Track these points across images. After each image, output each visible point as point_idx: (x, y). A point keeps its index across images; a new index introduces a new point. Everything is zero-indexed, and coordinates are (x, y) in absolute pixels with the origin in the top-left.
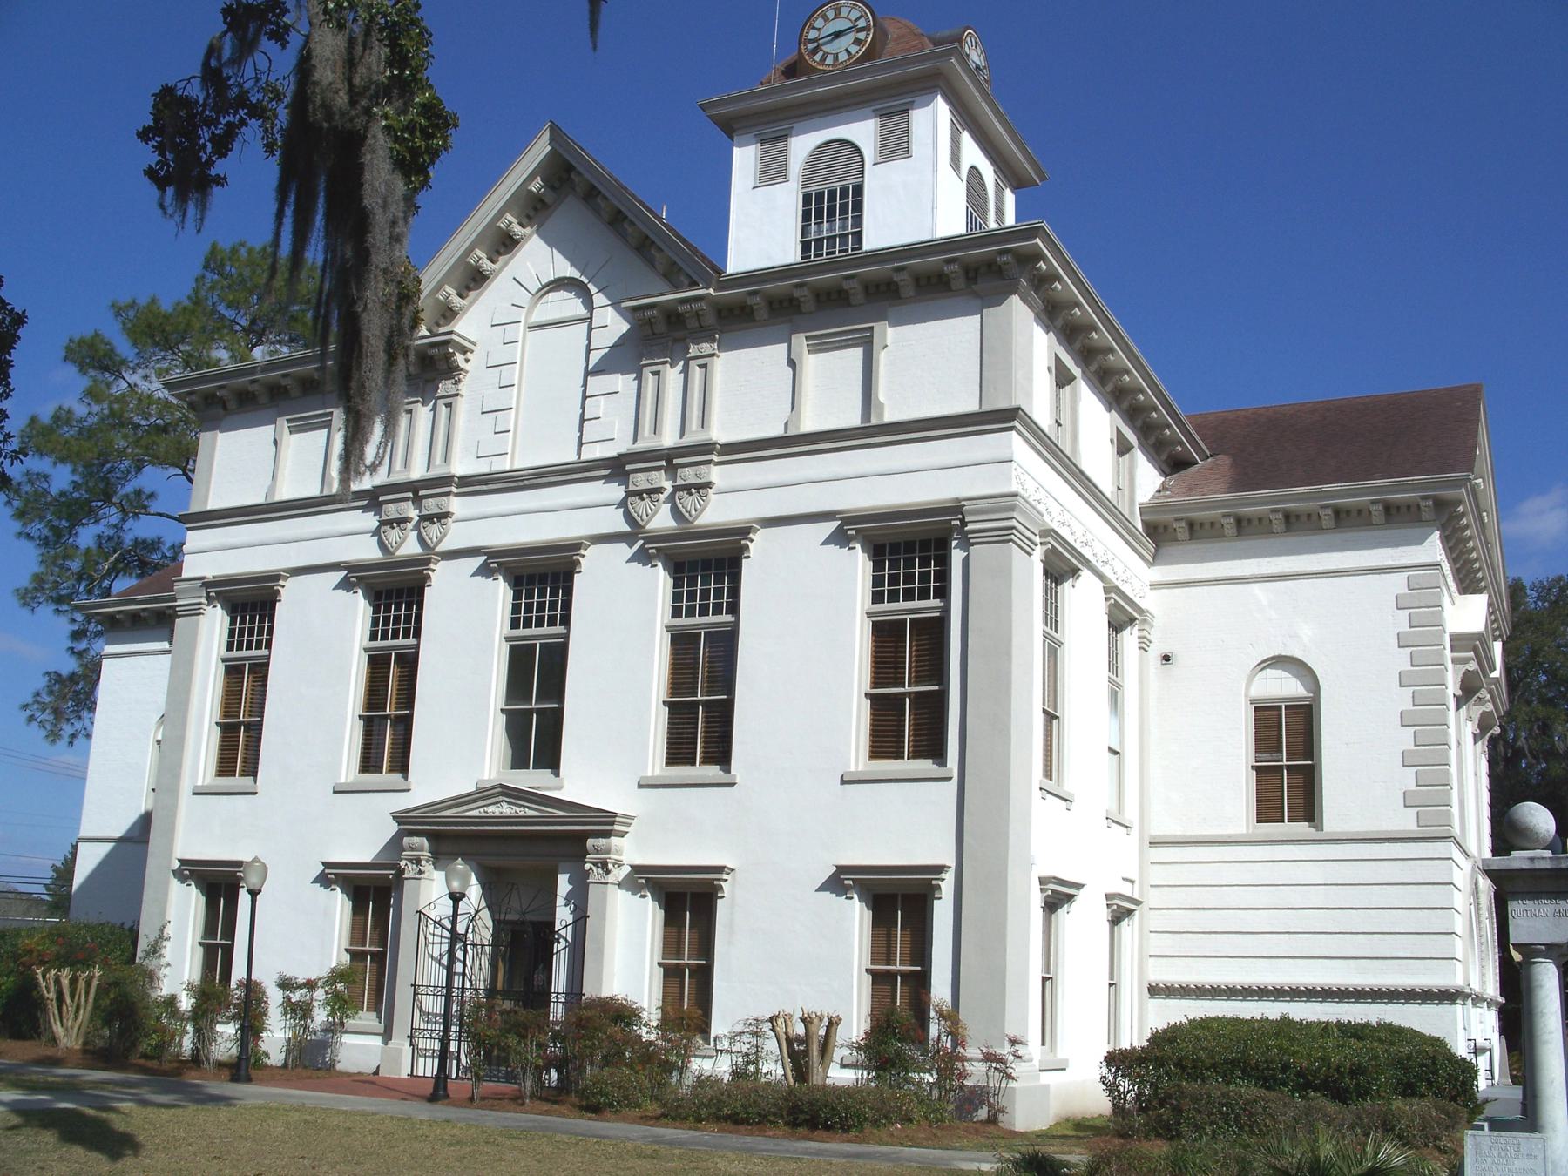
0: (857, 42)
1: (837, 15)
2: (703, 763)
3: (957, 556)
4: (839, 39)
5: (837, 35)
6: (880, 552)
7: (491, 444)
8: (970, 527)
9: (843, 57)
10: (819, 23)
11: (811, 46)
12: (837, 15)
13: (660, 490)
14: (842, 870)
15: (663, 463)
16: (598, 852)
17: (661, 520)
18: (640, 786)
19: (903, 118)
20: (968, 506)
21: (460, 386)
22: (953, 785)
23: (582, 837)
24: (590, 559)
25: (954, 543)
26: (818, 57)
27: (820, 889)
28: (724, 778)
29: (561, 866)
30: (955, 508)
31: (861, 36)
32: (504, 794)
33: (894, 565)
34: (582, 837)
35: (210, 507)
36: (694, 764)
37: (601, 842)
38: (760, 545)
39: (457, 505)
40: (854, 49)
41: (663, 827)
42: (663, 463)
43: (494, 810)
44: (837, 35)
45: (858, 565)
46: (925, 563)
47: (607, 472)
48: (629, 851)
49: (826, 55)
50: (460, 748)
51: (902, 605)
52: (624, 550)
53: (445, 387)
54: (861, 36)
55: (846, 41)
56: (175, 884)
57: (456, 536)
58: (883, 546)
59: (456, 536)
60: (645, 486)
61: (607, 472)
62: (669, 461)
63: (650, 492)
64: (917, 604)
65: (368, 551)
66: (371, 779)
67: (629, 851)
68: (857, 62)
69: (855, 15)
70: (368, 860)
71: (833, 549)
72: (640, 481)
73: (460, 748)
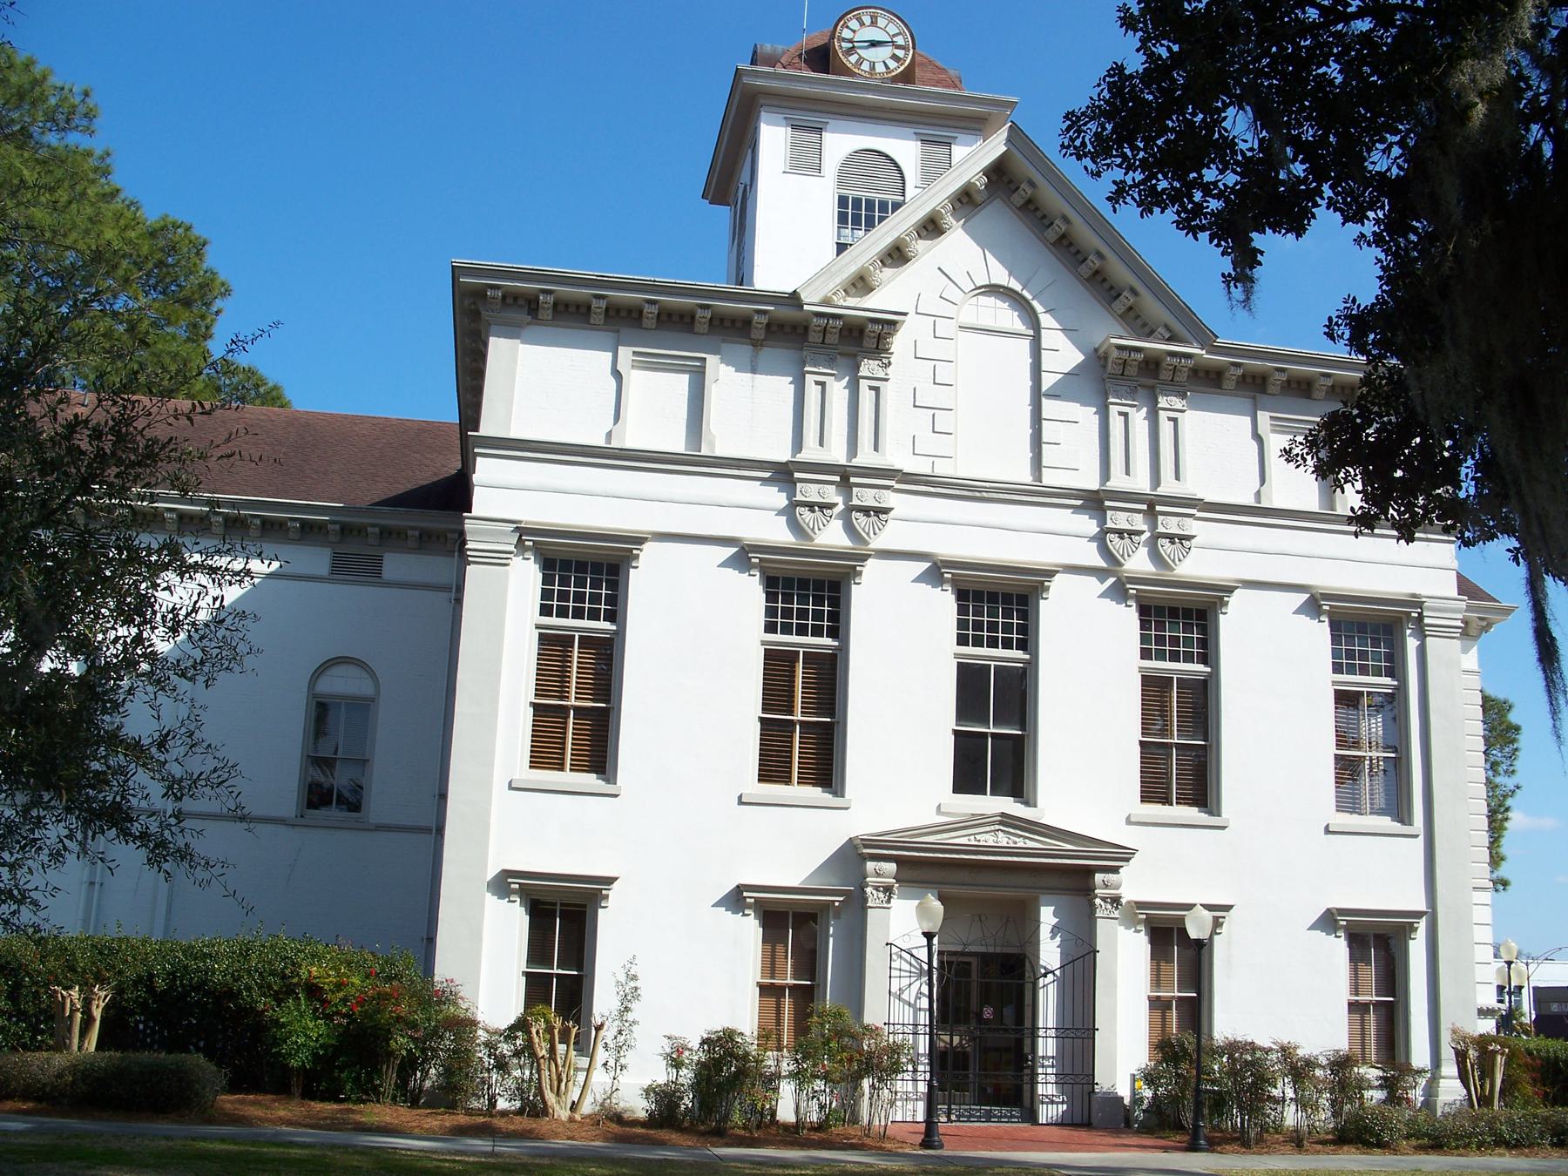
0: (895, 57)
1: (874, 23)
2: (802, 781)
3: (1412, 644)
4: (875, 44)
5: (874, 44)
6: (967, 596)
7: (928, 443)
8: (1427, 621)
9: (880, 68)
10: (854, 24)
11: (845, 45)
12: (874, 23)
13: (831, 506)
14: (740, 889)
15: (837, 479)
16: (1106, 887)
17: (1138, 562)
18: (1129, 822)
19: (814, 137)
20: (1428, 603)
21: (889, 370)
22: (1421, 840)
23: (1089, 872)
24: (1059, 586)
25: (1408, 632)
26: (853, 58)
27: (716, 905)
28: (609, 789)
29: (1043, 898)
30: (1416, 602)
31: (900, 53)
32: (1001, 823)
33: (564, 581)
34: (1089, 872)
35: (513, 435)
36: (562, 769)
37: (1111, 877)
38: (649, 554)
39: (1201, 530)
40: (892, 64)
41: (1166, 862)
42: (837, 479)
43: (989, 840)
44: (874, 44)
45: (944, 603)
46: (596, 584)
47: (1079, 502)
48: (1133, 884)
49: (861, 60)
50: (899, 769)
51: (985, 651)
52: (1094, 586)
53: (868, 367)
54: (900, 53)
55: (883, 53)
56: (491, 900)
57: (888, 536)
58: (554, 561)
59: (888, 536)
60: (1174, 530)
61: (1079, 502)
62: (1151, 506)
63: (1131, 533)
64: (1000, 652)
65: (777, 533)
66: (1156, 811)
67: (1133, 884)
68: (895, 79)
69: (893, 29)
70: (795, 884)
71: (925, 588)
72: (809, 492)
73: (899, 769)
